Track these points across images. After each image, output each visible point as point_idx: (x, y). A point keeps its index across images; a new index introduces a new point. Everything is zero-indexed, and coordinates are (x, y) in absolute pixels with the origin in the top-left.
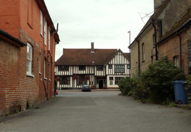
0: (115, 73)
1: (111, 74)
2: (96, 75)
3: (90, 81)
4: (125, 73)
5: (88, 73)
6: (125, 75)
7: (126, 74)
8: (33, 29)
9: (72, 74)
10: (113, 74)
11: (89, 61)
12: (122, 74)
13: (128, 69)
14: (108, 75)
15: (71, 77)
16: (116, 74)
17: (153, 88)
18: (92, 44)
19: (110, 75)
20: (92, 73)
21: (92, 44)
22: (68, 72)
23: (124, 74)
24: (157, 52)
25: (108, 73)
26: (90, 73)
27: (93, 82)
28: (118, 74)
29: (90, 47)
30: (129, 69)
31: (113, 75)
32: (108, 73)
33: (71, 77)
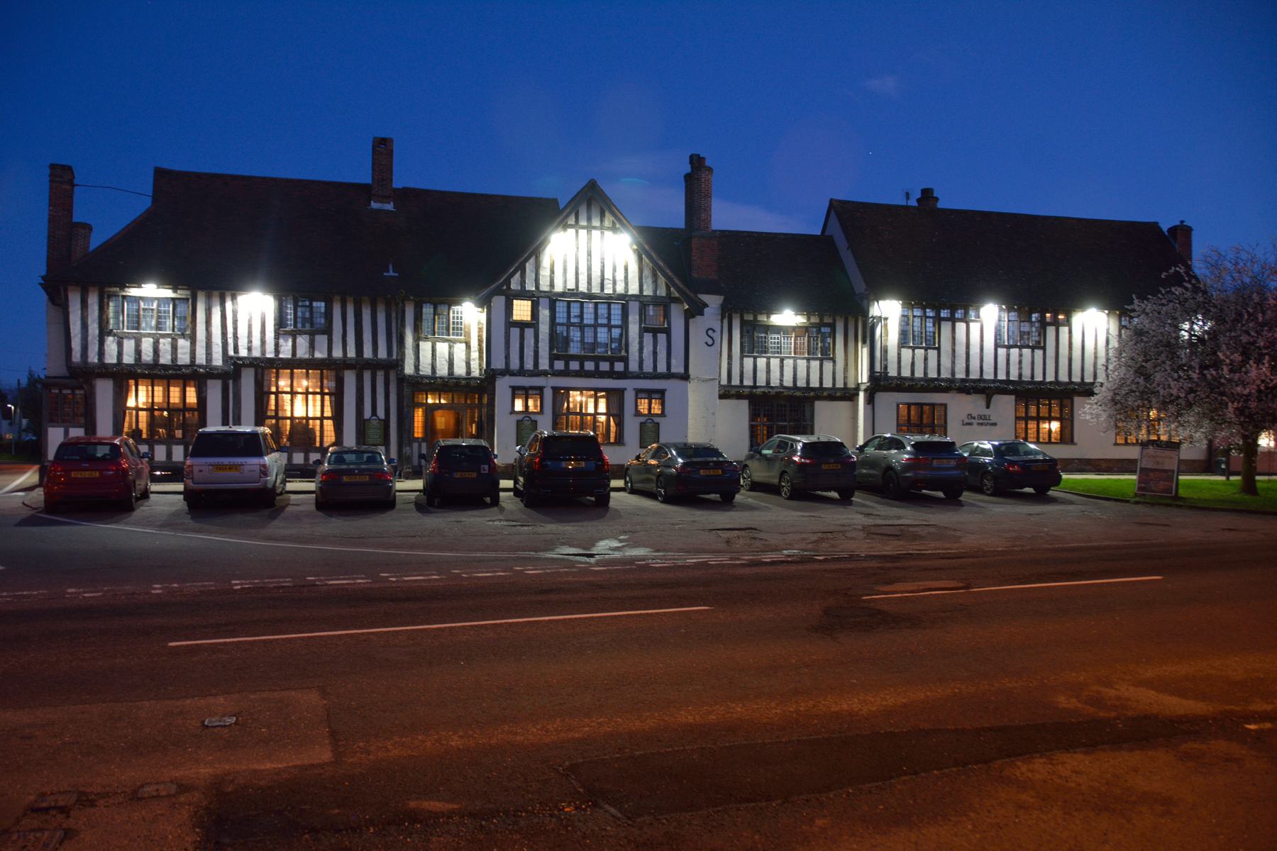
0: (553, 358)
1: (529, 365)
2: (409, 369)
3: (367, 413)
4: (625, 360)
5: (351, 353)
6: (625, 375)
7: (634, 366)
8: (998, 423)
9: (218, 361)
10: (544, 364)
11: (1230, 387)
12: (604, 366)
13: (647, 330)
14: (507, 372)
15: (745, 318)
16: (559, 365)
17: (727, 312)
18: (382, 148)
19: (522, 372)
20: (382, 354)
21: (382, 148)
22: (321, 340)
23: (619, 367)
24: (163, 797)
25: (507, 357)
26: (368, 353)
27: (386, 422)
28: (574, 366)
29: (363, 175)
30: (655, 332)
31: (545, 373)
32: (507, 357)
33: (745, 318)
